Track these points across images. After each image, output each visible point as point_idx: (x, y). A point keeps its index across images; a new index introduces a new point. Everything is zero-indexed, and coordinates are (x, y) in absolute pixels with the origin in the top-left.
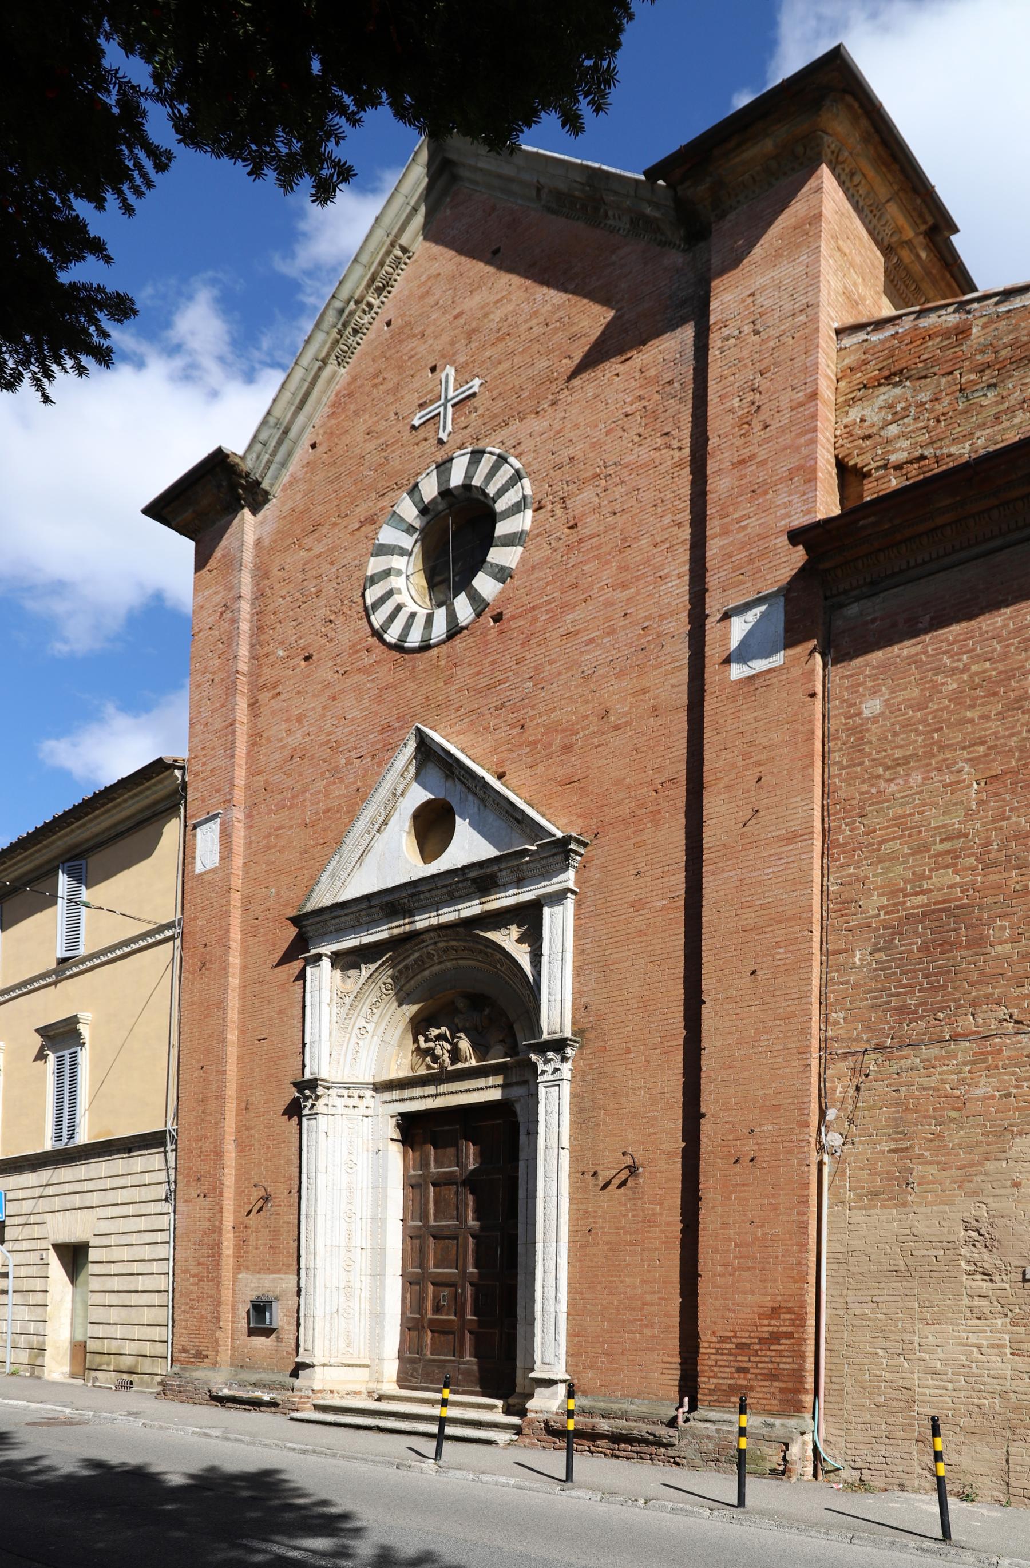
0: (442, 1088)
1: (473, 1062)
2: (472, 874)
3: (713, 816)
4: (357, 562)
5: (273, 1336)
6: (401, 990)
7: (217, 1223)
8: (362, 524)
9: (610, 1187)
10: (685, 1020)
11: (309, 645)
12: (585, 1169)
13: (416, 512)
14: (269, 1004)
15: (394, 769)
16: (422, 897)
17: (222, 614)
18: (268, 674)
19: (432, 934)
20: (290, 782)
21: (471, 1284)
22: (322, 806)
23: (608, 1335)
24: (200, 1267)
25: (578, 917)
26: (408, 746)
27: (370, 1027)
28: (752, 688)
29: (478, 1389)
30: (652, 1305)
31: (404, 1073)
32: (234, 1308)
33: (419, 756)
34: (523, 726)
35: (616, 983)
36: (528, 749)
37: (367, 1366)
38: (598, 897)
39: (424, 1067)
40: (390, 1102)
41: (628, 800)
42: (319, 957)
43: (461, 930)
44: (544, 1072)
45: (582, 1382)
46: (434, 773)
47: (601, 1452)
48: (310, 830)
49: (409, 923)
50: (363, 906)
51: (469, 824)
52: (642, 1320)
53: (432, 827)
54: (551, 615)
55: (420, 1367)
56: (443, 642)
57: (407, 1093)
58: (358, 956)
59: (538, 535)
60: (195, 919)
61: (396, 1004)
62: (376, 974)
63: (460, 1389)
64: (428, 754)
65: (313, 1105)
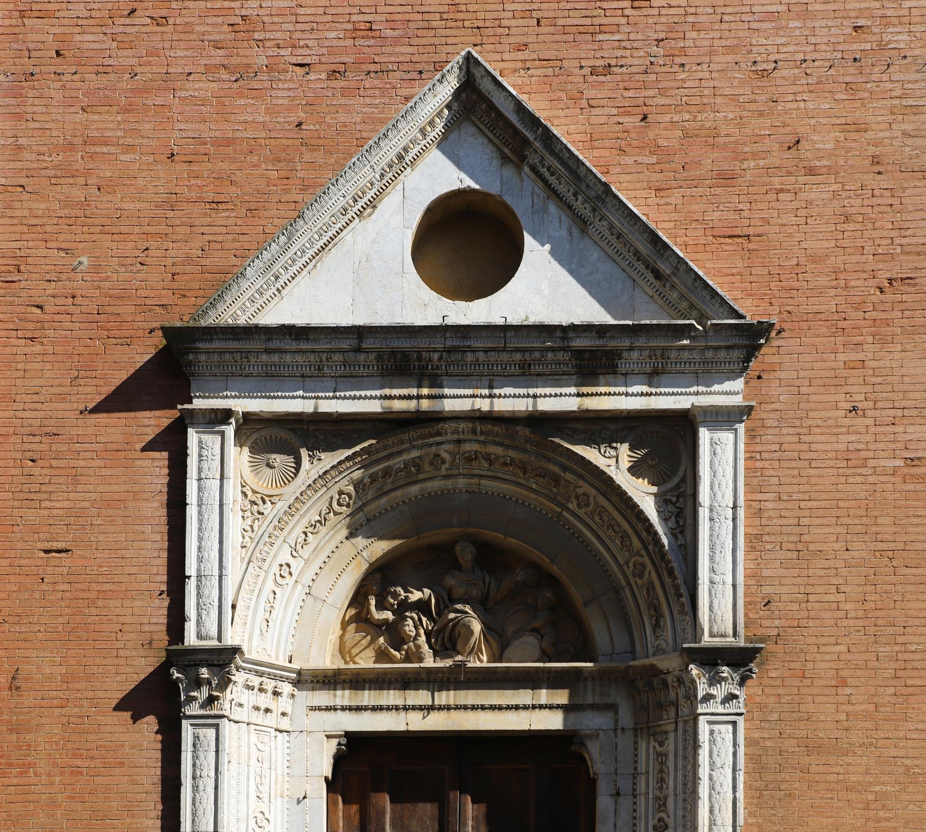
0: (443, 698)
1: (482, 661)
6: (360, 509)
16: (469, 357)
19: (462, 425)
20: (127, 59)
31: (325, 658)
33: (455, 106)
34: (645, 118)
35: (822, 572)
36: (654, 159)
38: (785, 431)
39: (370, 653)
40: (328, 709)
41: (832, 292)
44: (708, 698)
46: (475, 143)
49: (430, 397)
50: (345, 345)
51: (552, 253)
57: (367, 697)
58: (294, 431)
61: (345, 532)
62: (333, 473)
65: (211, 700)
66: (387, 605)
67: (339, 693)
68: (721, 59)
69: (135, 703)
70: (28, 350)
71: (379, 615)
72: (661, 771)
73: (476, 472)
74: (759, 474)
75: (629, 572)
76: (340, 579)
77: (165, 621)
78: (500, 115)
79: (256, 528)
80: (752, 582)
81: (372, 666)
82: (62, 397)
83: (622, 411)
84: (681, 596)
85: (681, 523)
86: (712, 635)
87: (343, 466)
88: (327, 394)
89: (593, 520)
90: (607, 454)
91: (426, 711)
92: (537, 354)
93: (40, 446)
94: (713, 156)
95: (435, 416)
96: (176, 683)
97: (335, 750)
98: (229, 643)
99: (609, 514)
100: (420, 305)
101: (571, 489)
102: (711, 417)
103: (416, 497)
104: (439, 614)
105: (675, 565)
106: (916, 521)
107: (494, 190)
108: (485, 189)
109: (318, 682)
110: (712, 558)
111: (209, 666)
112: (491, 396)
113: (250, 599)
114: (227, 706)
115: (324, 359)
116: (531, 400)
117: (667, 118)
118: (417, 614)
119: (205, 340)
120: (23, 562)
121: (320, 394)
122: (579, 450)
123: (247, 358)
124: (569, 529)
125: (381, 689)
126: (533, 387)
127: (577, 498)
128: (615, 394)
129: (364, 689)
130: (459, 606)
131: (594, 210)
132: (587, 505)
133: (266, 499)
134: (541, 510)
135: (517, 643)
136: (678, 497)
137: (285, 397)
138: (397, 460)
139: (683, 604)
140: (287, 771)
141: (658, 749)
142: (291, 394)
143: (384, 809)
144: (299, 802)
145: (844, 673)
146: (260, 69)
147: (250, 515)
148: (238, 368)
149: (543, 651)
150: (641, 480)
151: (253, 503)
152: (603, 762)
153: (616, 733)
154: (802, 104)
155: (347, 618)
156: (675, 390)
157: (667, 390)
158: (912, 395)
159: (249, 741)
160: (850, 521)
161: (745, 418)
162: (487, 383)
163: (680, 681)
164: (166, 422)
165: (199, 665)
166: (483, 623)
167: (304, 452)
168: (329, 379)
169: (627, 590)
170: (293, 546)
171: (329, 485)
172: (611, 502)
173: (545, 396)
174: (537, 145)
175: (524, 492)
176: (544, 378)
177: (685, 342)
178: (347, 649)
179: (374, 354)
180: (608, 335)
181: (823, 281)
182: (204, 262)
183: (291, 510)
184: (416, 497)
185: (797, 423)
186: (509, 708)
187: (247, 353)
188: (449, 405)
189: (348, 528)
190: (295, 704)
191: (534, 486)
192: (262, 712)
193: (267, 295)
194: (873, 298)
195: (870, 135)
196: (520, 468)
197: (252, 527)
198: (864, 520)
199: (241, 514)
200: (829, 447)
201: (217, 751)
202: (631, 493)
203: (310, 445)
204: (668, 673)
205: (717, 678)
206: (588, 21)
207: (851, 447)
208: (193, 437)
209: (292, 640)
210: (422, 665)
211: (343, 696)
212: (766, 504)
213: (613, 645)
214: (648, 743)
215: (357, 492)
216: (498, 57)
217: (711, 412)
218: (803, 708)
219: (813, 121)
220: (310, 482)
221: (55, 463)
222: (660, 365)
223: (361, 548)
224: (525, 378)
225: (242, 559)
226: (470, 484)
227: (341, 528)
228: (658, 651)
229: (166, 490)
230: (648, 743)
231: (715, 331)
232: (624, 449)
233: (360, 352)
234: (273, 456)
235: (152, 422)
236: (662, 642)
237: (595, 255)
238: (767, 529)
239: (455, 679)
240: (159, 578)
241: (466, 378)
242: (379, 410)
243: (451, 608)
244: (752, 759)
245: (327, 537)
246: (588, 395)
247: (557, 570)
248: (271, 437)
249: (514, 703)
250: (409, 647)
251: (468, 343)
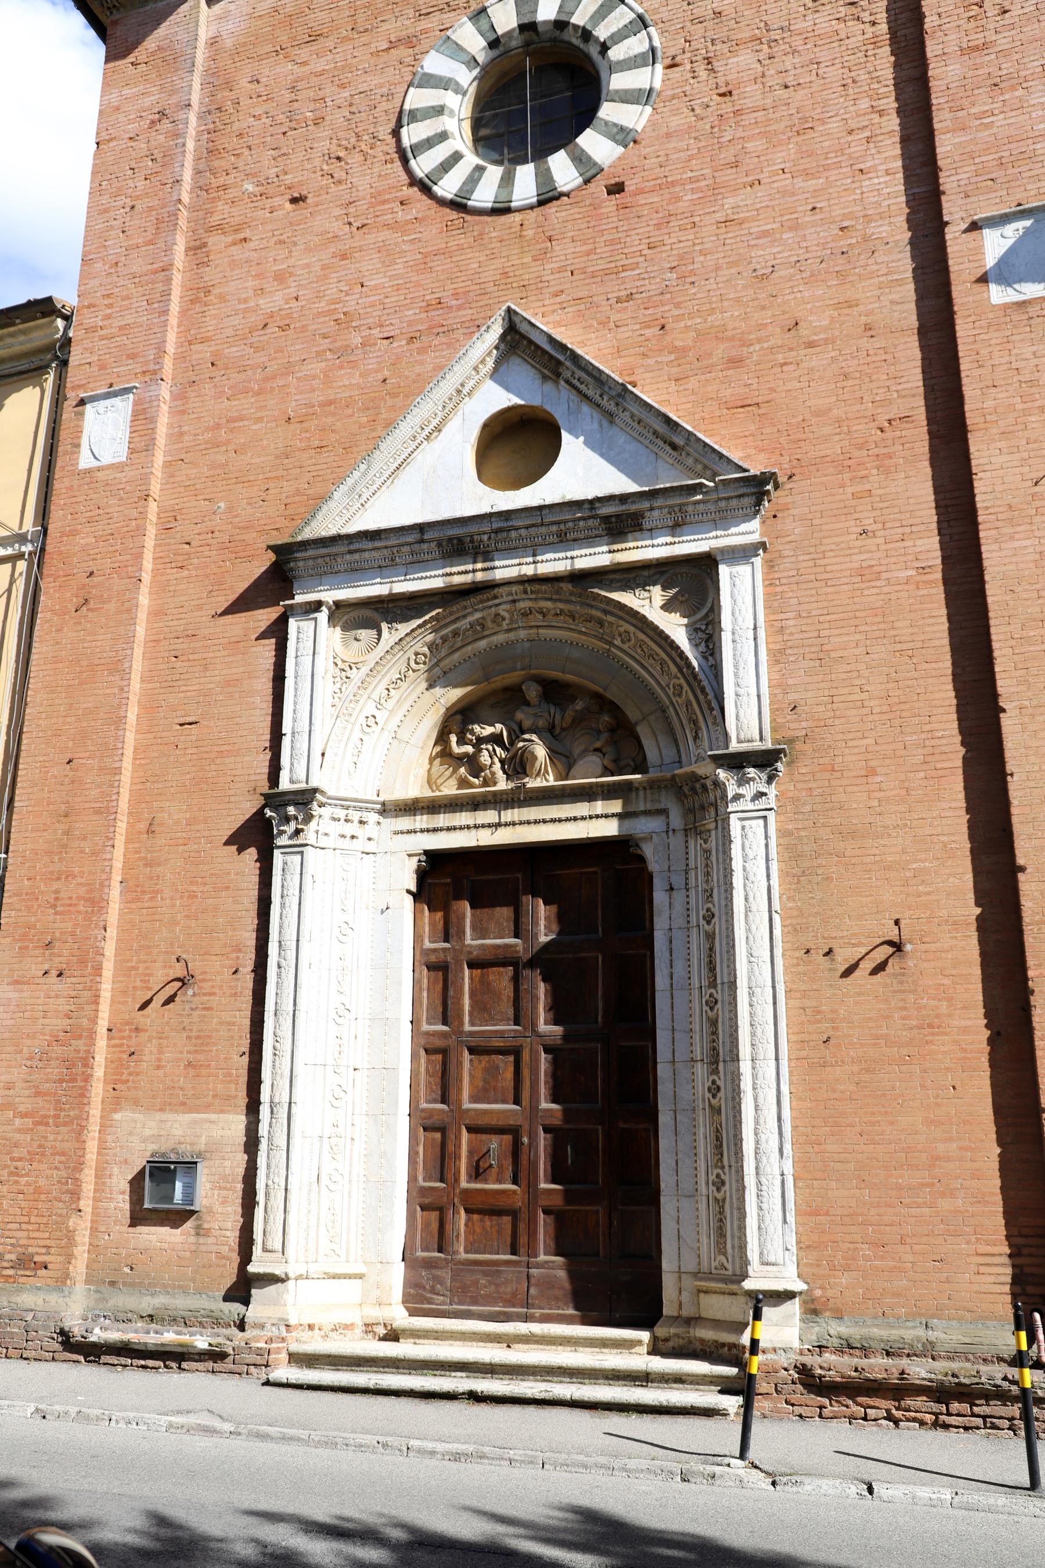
0: (508, 815)
1: (551, 780)
2: (605, 510)
3: (986, 468)
4: (385, 90)
5: (189, 1224)
6: (437, 664)
7: (85, 1022)
8: (392, 45)
9: (857, 973)
10: (961, 732)
11: (301, 183)
12: (810, 945)
13: (483, 43)
14: (206, 669)
15: (467, 359)
16: (513, 534)
17: (153, 122)
18: (222, 211)
19: (514, 588)
20: (261, 358)
21: (546, 1130)
22: (318, 397)
23: (873, 1212)
24: (39, 1099)
25: (769, 584)
26: (491, 331)
28: (1025, 317)
29: (571, 1311)
30: (948, 1159)
31: (415, 789)
32: (101, 1174)
33: (502, 346)
34: (663, 327)
35: (845, 676)
37: (360, 1276)
38: (801, 558)
39: (453, 782)
40: (409, 832)
41: (837, 438)
42: (317, 606)
43: (567, 587)
44: (737, 797)
45: (830, 1293)
46: (522, 370)
47: (914, 1420)
48: (294, 427)
49: (483, 570)
51: (585, 443)
52: (933, 1185)
53: (518, 442)
54: (700, 195)
55: (446, 1275)
56: (531, 207)
57: (442, 820)
58: (376, 610)
59: (673, 97)
60: (74, 533)
61: (425, 685)
62: (408, 639)
63: (537, 1312)
64: (517, 341)
65: (298, 832)
67: (418, 818)
68: (725, 273)
69: (239, 839)
70: (178, 576)
71: (457, 750)
72: (707, 866)
75: (671, 692)
78: (537, 347)
82: (199, 607)
92: (570, 524)
93: (181, 645)
94: (722, 346)
96: (269, 822)
100: (477, 498)
104: (512, 743)
105: (705, 683)
106: (931, 621)
107: (536, 402)
108: (530, 403)
110: (736, 675)
111: (296, 804)
116: (569, 561)
117: (682, 324)
120: (164, 734)
122: (616, 596)
125: (454, 812)
127: (620, 635)
130: (526, 736)
131: (617, 405)
132: (629, 640)
136: (707, 625)
143: (464, 914)
144: (382, 912)
145: (872, 764)
146: (357, 347)
154: (799, 295)
158: (917, 514)
160: (867, 628)
167: (384, 626)
174: (568, 363)
177: (699, 497)
181: (827, 430)
182: (309, 492)
185: (812, 550)
188: (500, 574)
193: (352, 510)
194: (874, 438)
195: (861, 308)
198: (882, 626)
200: (843, 566)
202: (662, 626)
206: (613, 265)
207: (864, 564)
208: (293, 624)
216: (540, 304)
218: (834, 798)
219: (809, 306)
221: (191, 657)
228: (699, 759)
237: (621, 439)
242: (442, 585)
249: (572, 815)
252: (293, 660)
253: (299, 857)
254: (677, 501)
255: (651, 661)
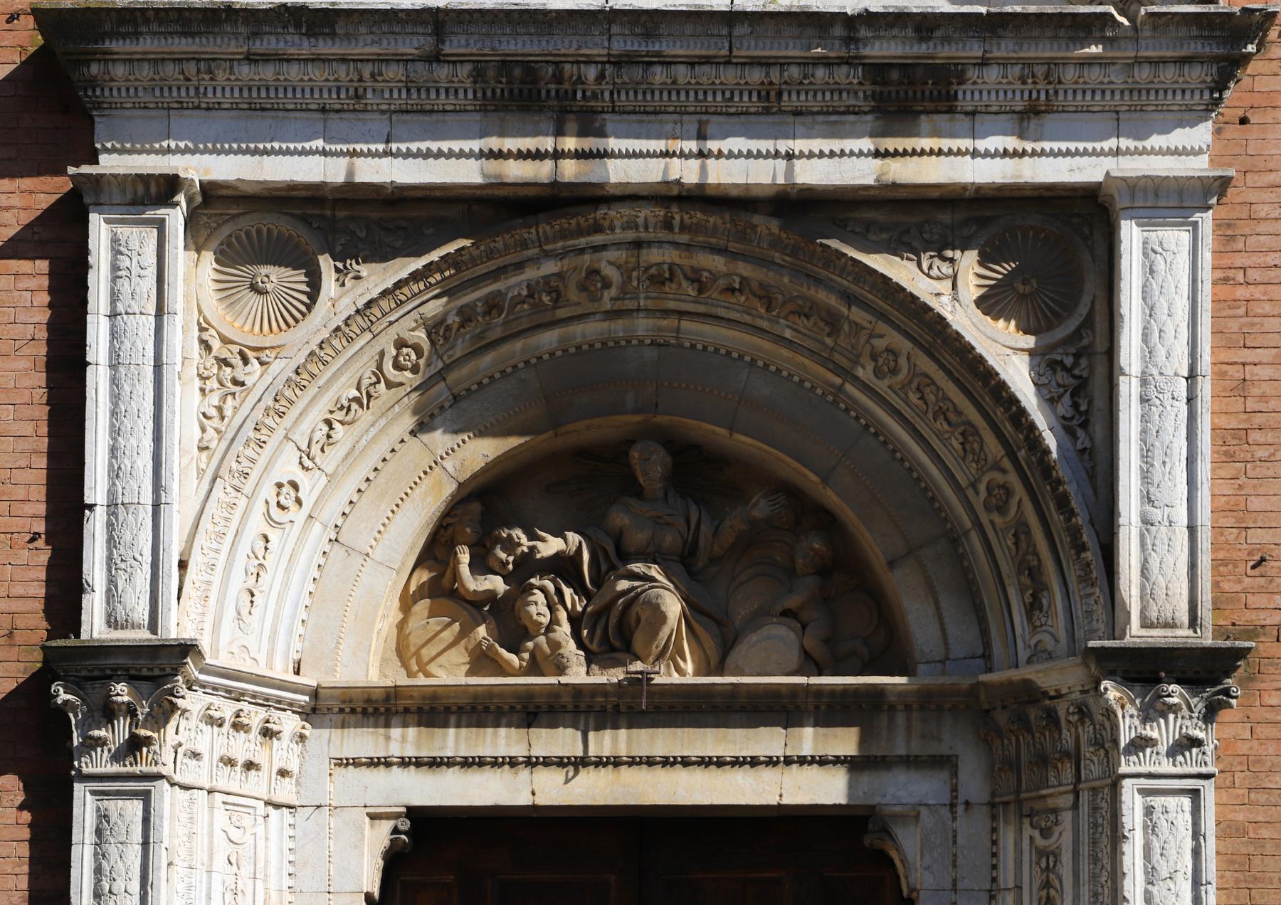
0: (605, 742)
1: (683, 672)
6: (440, 376)
16: (659, 75)
19: (645, 213)
27: (310, 485)
31: (367, 666)
40: (373, 763)
43: (767, 225)
44: (93, 744)
49: (580, 155)
57: (452, 741)
58: (306, 220)
61: (409, 422)
65: (135, 745)
66: (493, 564)
67: (396, 732)
72: (1047, 885)
73: (672, 305)
74: (1242, 311)
75: (978, 501)
76: (399, 513)
77: (42, 592)
79: (228, 412)
80: (1229, 522)
81: (463, 680)
83: (964, 187)
84: (1082, 548)
85: (1083, 408)
86: (1146, 624)
87: (405, 290)
88: (373, 147)
89: (906, 401)
90: (935, 272)
91: (571, 768)
92: (795, 71)
95: (589, 193)
96: (61, 713)
97: (386, 843)
98: (173, 636)
99: (938, 388)
101: (863, 339)
102: (1145, 199)
103: (552, 354)
104: (598, 580)
105: (1071, 488)
109: (353, 711)
110: (1146, 476)
111: (132, 678)
112: (701, 155)
113: (217, 551)
114: (167, 756)
115: (367, 75)
116: (781, 164)
118: (552, 580)
119: (124, 36)
121: (358, 147)
122: (879, 263)
123: (210, 72)
124: (857, 418)
125: (481, 724)
126: (787, 138)
127: (874, 357)
128: (950, 152)
129: (445, 725)
130: (638, 567)
132: (894, 371)
133: (250, 354)
134: (802, 381)
135: (754, 638)
136: (1077, 356)
137: (288, 152)
138: (513, 281)
139: (1088, 565)
140: (288, 882)
141: (1040, 842)
142: (299, 146)
147: (216, 385)
148: (192, 92)
149: (806, 654)
150: (1001, 323)
151: (224, 362)
152: (928, 868)
153: (953, 813)
155: (413, 588)
156: (1072, 146)
157: (1056, 146)
159: (211, 825)
161: (1214, 201)
162: (693, 128)
163: (1083, 712)
164: (44, 201)
165: (110, 678)
166: (685, 599)
168: (377, 116)
169: (974, 537)
170: (304, 447)
171: (377, 328)
172: (942, 366)
173: (811, 155)
175: (767, 345)
176: (809, 119)
177: (1095, 49)
178: (413, 649)
179: (468, 68)
180: (938, 34)
183: (300, 378)
184: (552, 354)
186: (737, 762)
187: (209, 63)
188: (619, 172)
189: (415, 412)
190: (306, 753)
191: (788, 334)
192: (238, 769)
196: (760, 298)
197: (220, 409)
199: (197, 383)
201: (145, 844)
202: (983, 347)
203: (339, 248)
204: (1059, 696)
205: (1159, 706)
208: (100, 230)
209: (301, 630)
210: (564, 680)
211: (404, 739)
212: (1257, 369)
213: (946, 643)
214: (1020, 832)
215: (433, 343)
217: (1145, 190)
220: (338, 321)
222: (1043, 97)
223: (441, 452)
224: (770, 119)
225: (201, 473)
226: (660, 329)
227: (400, 414)
228: (1039, 654)
229: (43, 334)
230: (1020, 832)
231: (1155, 28)
232: (968, 261)
233: (438, 61)
234: (264, 270)
235: (15, 201)
236: (1046, 638)
238: (1258, 419)
239: (630, 707)
240: (29, 509)
241: (652, 117)
242: (478, 180)
243: (621, 571)
244: (1232, 862)
245: (373, 431)
246: (896, 154)
247: (835, 498)
248: (259, 231)
250: (536, 645)
251: (657, 48)
252: (104, 324)
253: (136, 806)
254: (1046, 51)
255: (941, 425)
